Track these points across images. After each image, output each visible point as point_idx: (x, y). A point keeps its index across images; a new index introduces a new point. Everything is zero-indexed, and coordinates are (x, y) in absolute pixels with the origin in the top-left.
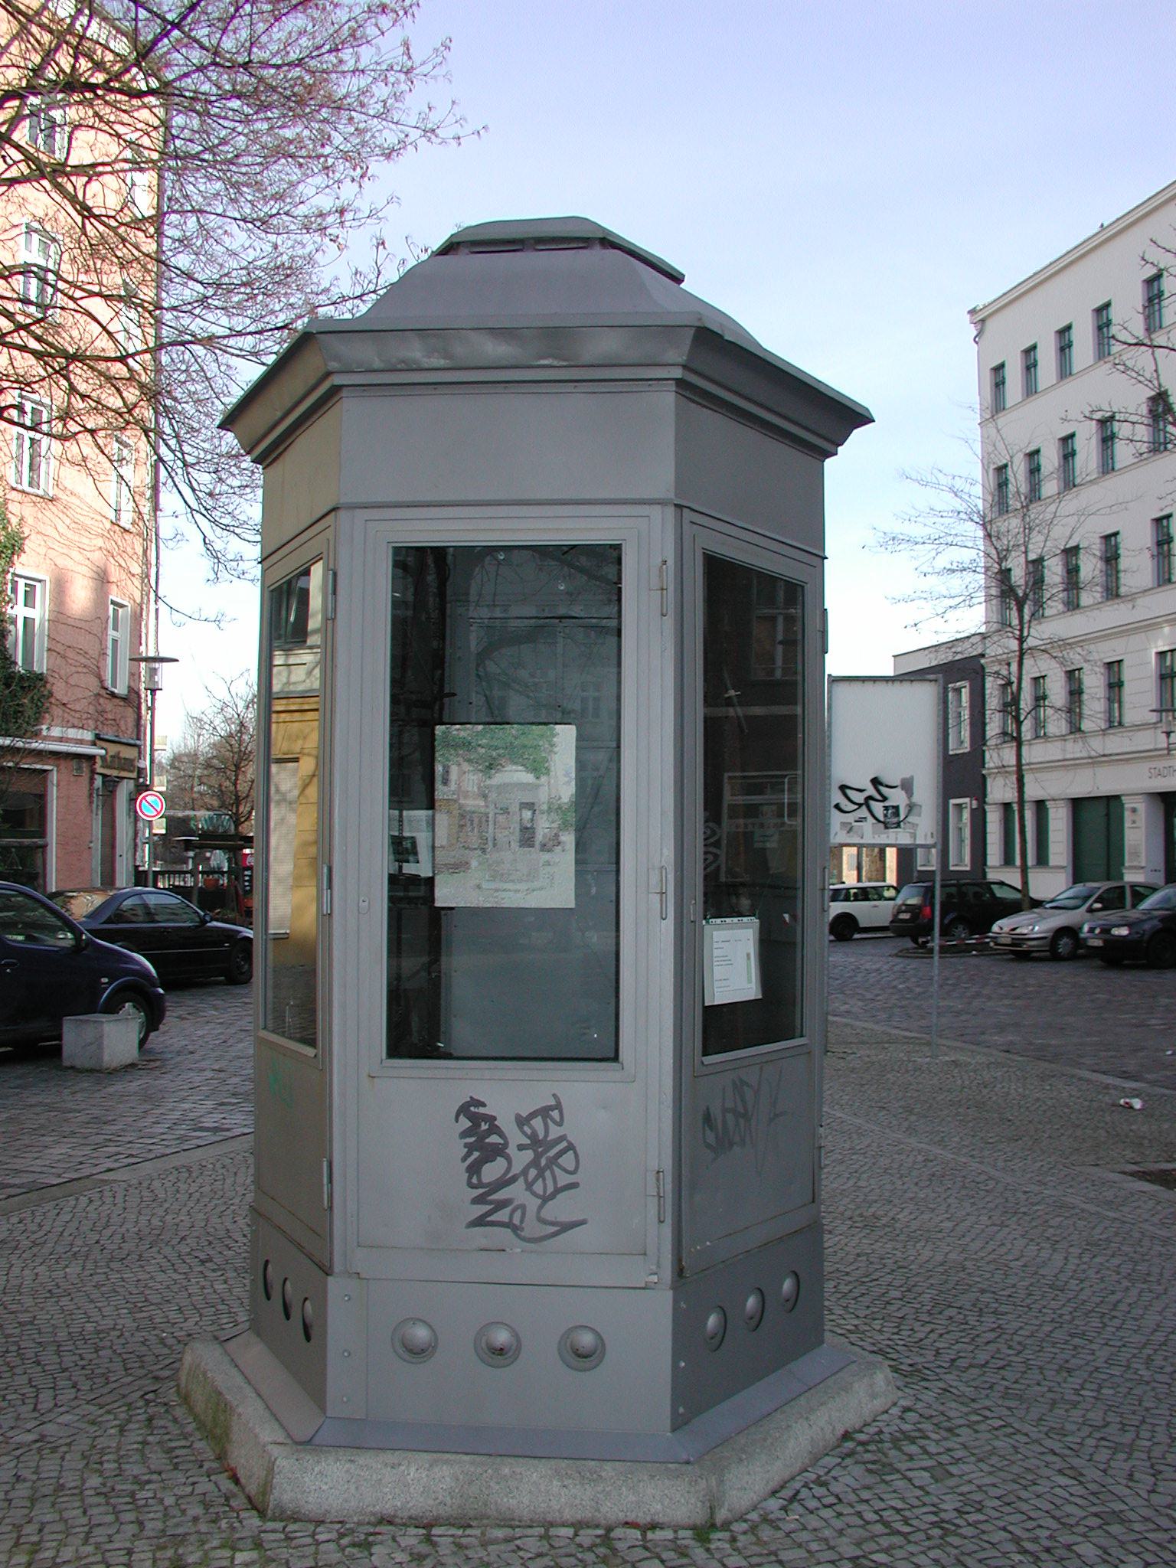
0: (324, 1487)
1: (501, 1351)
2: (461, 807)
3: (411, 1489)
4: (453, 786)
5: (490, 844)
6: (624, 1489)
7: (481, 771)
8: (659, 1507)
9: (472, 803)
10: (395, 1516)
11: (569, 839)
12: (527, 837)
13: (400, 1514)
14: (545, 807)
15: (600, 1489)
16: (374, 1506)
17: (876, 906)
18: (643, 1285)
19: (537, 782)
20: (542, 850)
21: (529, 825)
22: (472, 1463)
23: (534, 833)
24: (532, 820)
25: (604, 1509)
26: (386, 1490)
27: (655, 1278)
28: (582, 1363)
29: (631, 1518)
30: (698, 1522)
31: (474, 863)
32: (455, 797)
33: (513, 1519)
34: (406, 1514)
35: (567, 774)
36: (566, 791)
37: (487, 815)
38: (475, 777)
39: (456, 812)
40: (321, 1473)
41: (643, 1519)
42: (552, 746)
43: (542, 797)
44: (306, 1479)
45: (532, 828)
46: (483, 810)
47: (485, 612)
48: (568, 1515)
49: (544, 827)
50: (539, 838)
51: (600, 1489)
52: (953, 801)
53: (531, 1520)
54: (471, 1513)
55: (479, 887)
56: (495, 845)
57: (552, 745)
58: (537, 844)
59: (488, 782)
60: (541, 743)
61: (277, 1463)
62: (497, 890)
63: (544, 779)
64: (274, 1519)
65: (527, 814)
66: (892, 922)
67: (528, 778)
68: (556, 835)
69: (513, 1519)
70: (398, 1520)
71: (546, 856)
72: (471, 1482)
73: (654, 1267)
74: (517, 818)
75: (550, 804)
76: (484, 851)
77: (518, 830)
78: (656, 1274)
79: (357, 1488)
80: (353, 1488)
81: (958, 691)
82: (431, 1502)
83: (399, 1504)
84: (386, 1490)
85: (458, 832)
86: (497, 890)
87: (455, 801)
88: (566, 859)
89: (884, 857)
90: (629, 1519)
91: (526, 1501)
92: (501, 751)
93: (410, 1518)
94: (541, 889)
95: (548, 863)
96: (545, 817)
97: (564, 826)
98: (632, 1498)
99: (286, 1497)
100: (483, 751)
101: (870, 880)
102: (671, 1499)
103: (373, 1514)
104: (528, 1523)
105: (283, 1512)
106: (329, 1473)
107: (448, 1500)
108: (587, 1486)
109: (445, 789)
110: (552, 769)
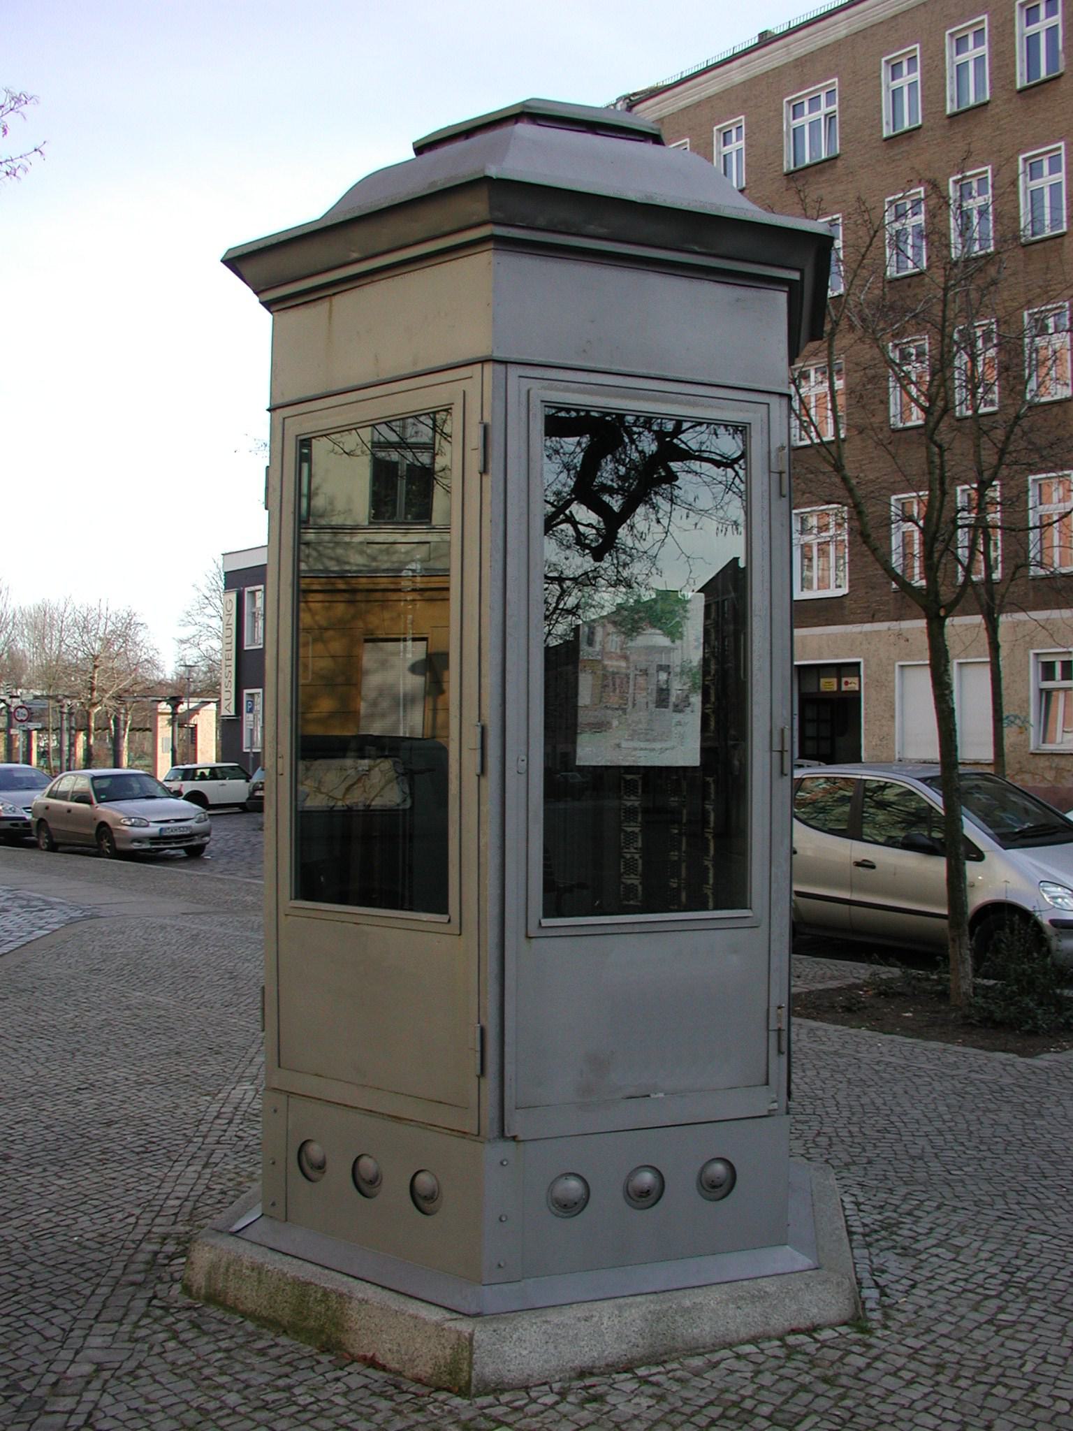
0: (524, 1353)
1: (645, 1193)
2: (604, 668)
3: (606, 1338)
4: (598, 647)
5: (630, 704)
6: (787, 1300)
7: (624, 633)
8: (816, 1310)
9: (613, 664)
10: (593, 1367)
11: (696, 699)
12: (662, 698)
13: (597, 1364)
14: (678, 670)
15: (767, 1304)
16: (573, 1361)
17: (223, 785)
18: (766, 1113)
19: (672, 645)
20: (674, 711)
21: (665, 687)
22: (651, 1302)
23: (668, 694)
24: (667, 681)
25: (772, 1322)
26: (582, 1343)
27: (775, 1106)
28: (719, 1192)
29: (795, 1324)
30: (846, 1318)
31: (615, 723)
32: (599, 657)
33: (698, 1348)
34: (603, 1363)
35: (696, 640)
36: (696, 655)
37: (627, 676)
38: (618, 639)
39: (600, 672)
40: (519, 1339)
41: (804, 1323)
42: (686, 611)
43: (675, 660)
44: (507, 1348)
45: (668, 690)
46: (624, 671)
47: (949, 474)
48: (744, 1333)
49: (677, 688)
50: (673, 699)
51: (767, 1304)
52: (246, 691)
53: (713, 1345)
54: (661, 1350)
55: (619, 746)
56: (634, 705)
57: (686, 611)
58: (671, 705)
59: (630, 644)
60: (676, 608)
61: (475, 1337)
62: (635, 749)
63: (678, 642)
64: (479, 1394)
65: (663, 676)
66: (249, 799)
67: (662, 641)
68: (687, 697)
69: (698, 1348)
70: (595, 1371)
71: (678, 717)
72: (658, 1320)
73: (775, 1096)
74: (654, 680)
75: (682, 667)
76: (624, 711)
77: (655, 692)
78: (775, 1102)
79: (556, 1347)
80: (551, 1346)
81: (253, 593)
82: (624, 1346)
83: (595, 1354)
84: (582, 1343)
85: (602, 692)
86: (635, 749)
87: (599, 661)
88: (692, 720)
89: (196, 740)
90: (794, 1327)
91: (707, 1329)
92: (642, 615)
93: (607, 1365)
94: (673, 748)
95: (679, 723)
96: (678, 678)
97: (693, 689)
98: (795, 1307)
99: (488, 1371)
100: (626, 613)
101: (129, 767)
102: (824, 1301)
103: (573, 1369)
104: (712, 1348)
105: (487, 1385)
106: (528, 1338)
107: (641, 1342)
108: (757, 1304)
109: (590, 649)
110: (685, 633)
